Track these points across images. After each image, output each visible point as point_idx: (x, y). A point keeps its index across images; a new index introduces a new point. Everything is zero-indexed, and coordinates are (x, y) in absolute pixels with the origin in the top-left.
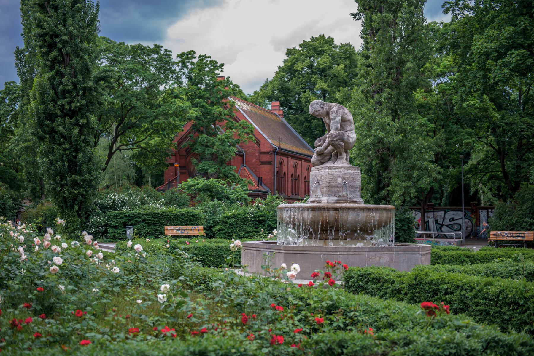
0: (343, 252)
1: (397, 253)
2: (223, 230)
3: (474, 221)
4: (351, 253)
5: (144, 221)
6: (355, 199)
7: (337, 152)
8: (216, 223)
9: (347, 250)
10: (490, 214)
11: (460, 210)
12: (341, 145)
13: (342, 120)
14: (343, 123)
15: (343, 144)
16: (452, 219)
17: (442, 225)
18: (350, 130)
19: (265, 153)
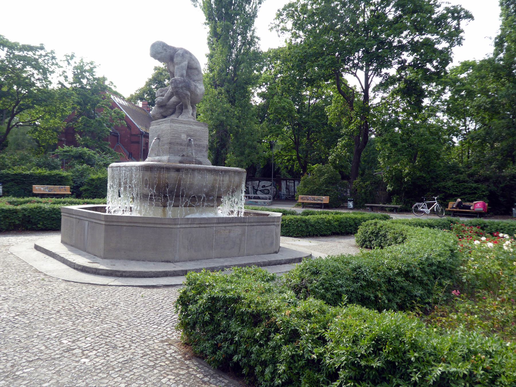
0: (185, 224)
1: (249, 224)
2: (88, 190)
3: (278, 188)
4: (195, 226)
5: (12, 180)
6: (201, 159)
7: (182, 105)
8: (82, 184)
9: (190, 222)
10: (288, 183)
11: (270, 180)
12: (187, 95)
13: (188, 67)
14: (189, 71)
15: (189, 94)
16: (264, 186)
17: (257, 190)
18: (198, 81)
19: (134, 135)
